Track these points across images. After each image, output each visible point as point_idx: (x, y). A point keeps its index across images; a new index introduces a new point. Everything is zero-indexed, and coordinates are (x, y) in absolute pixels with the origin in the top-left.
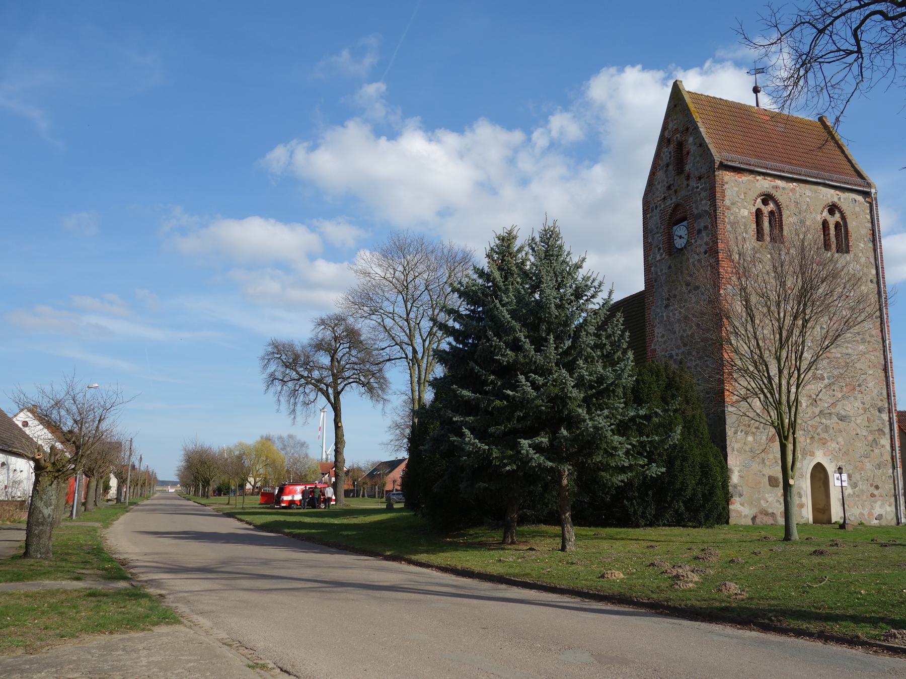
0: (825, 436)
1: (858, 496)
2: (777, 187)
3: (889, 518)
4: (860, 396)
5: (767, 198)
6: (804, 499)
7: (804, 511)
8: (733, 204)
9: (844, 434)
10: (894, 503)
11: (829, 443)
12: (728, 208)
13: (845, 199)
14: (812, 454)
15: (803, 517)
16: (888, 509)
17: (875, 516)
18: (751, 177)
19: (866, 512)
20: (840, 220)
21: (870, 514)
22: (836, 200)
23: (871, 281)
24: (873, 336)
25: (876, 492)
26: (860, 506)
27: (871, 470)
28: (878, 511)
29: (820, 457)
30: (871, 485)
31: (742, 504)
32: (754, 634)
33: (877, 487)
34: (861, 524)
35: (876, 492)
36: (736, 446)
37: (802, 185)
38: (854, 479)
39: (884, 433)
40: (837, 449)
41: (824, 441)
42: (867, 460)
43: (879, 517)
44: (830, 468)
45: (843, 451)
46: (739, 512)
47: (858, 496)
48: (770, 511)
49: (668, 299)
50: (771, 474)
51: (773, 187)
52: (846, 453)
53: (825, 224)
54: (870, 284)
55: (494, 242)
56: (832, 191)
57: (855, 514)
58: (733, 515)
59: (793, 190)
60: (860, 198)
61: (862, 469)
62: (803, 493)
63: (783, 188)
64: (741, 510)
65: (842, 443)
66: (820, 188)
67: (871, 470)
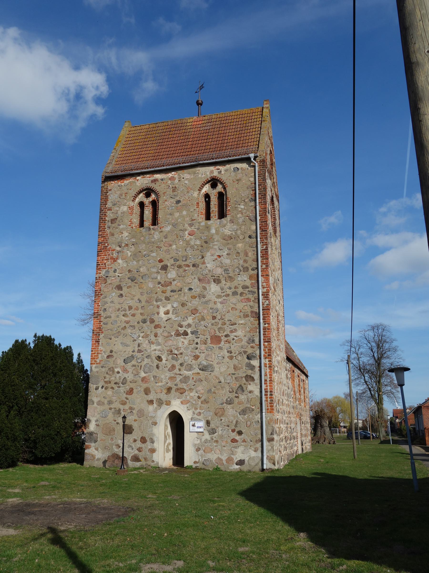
0: (184, 386)
1: (217, 441)
2: (155, 181)
3: (253, 464)
5: (214, 182)
6: (156, 445)
8: (114, 205)
9: (204, 383)
10: (260, 449)
11: (186, 393)
12: (110, 209)
13: (226, 170)
14: (168, 403)
15: (153, 461)
16: (253, 454)
17: (236, 461)
18: (132, 180)
19: (224, 458)
20: (222, 190)
21: (229, 460)
22: (216, 174)
23: (250, 237)
24: (247, 287)
25: (238, 438)
26: (218, 451)
28: (239, 455)
29: (176, 405)
30: (233, 431)
31: (97, 449)
32: (299, 372)
33: (240, 433)
34: (217, 469)
35: (238, 438)
36: (95, 400)
37: (180, 172)
38: (212, 425)
39: (253, 379)
41: (182, 391)
42: (229, 406)
43: (241, 462)
44: (186, 416)
45: (202, 399)
46: (93, 456)
51: (152, 181)
53: (207, 196)
54: (247, 239)
56: (212, 168)
57: (217, 456)
58: (87, 457)
59: (172, 179)
60: (244, 165)
62: (155, 439)
63: (162, 180)
64: (95, 453)
66: (199, 169)
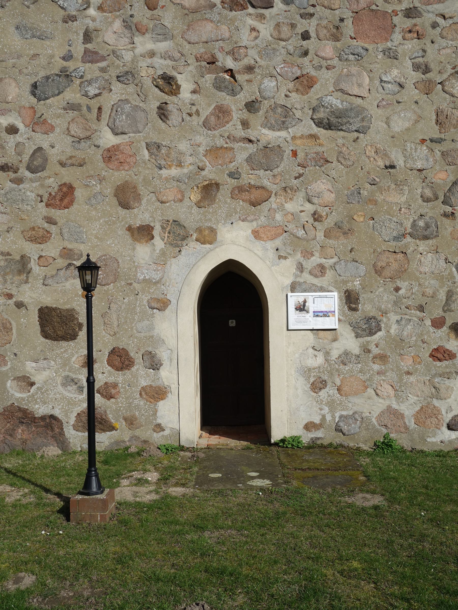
1: (382, 358)
4: (411, 45)
6: (166, 375)
7: (166, 412)
9: (336, 169)
11: (273, 202)
14: (208, 237)
15: (159, 428)
17: (448, 417)
19: (409, 408)
21: (427, 414)
26: (387, 390)
27: (440, 278)
30: (438, 323)
38: (366, 307)
40: (306, 218)
41: (255, 195)
42: (423, 246)
45: (329, 222)
47: (382, 358)
48: (41, 410)
49: (255, 543)
50: (48, 301)
52: (342, 229)
55: (298, 312)
61: (401, 273)
62: (163, 354)
65: (329, 197)
67: (440, 278)
